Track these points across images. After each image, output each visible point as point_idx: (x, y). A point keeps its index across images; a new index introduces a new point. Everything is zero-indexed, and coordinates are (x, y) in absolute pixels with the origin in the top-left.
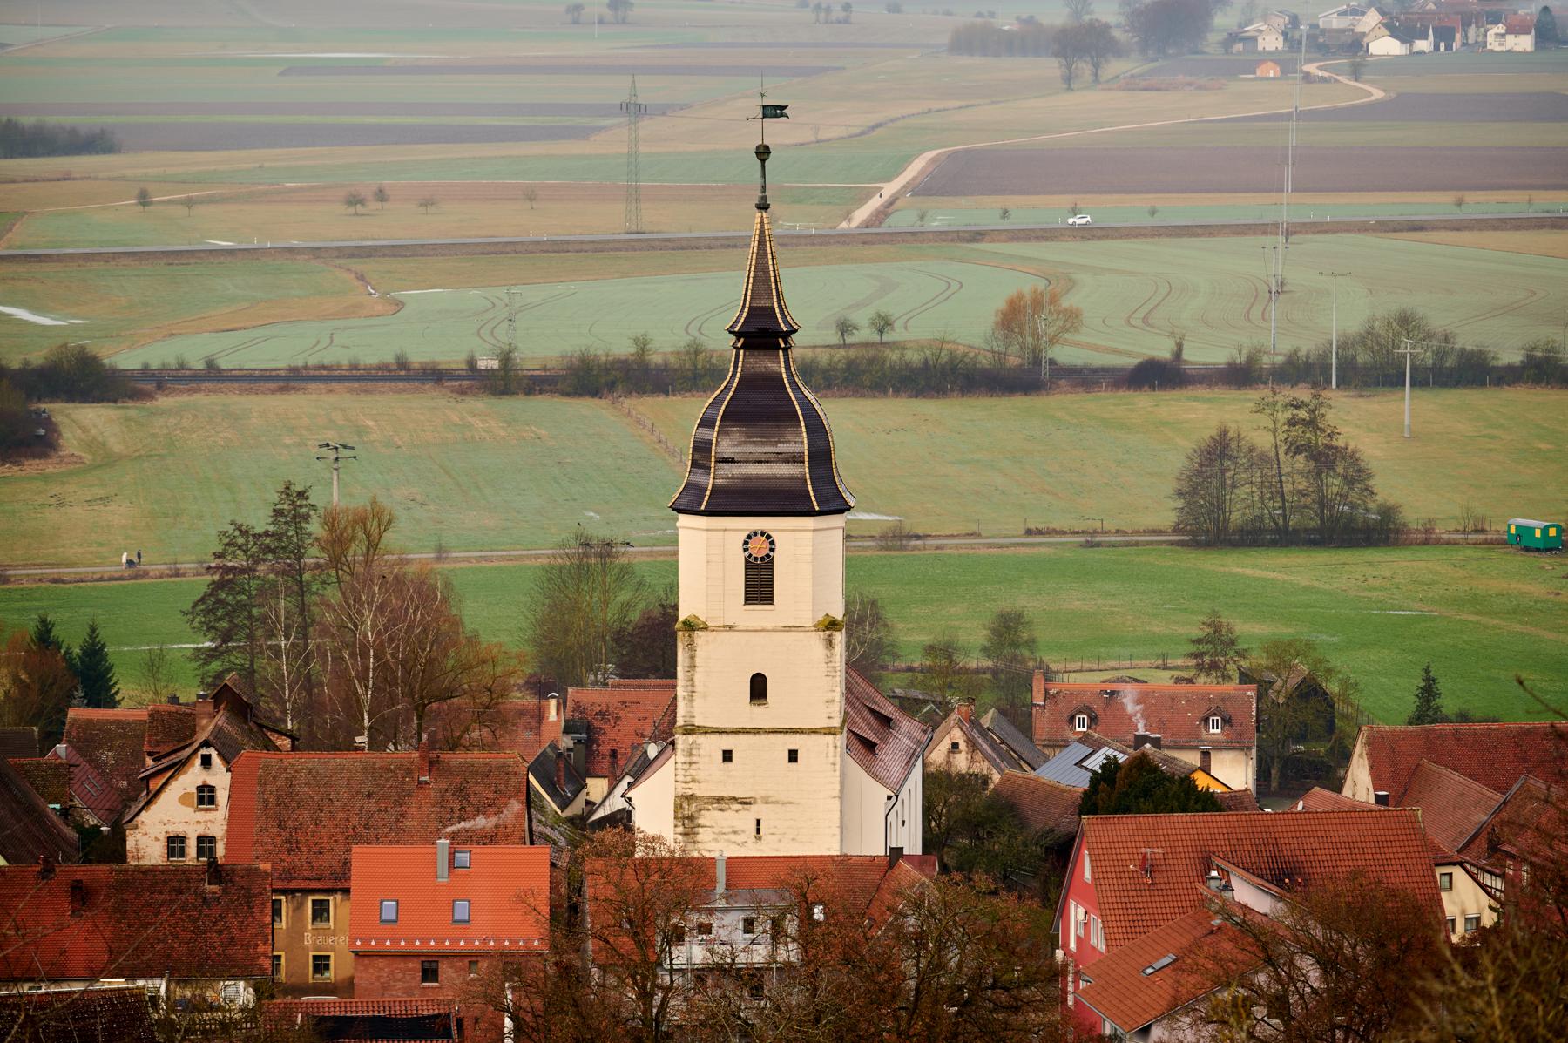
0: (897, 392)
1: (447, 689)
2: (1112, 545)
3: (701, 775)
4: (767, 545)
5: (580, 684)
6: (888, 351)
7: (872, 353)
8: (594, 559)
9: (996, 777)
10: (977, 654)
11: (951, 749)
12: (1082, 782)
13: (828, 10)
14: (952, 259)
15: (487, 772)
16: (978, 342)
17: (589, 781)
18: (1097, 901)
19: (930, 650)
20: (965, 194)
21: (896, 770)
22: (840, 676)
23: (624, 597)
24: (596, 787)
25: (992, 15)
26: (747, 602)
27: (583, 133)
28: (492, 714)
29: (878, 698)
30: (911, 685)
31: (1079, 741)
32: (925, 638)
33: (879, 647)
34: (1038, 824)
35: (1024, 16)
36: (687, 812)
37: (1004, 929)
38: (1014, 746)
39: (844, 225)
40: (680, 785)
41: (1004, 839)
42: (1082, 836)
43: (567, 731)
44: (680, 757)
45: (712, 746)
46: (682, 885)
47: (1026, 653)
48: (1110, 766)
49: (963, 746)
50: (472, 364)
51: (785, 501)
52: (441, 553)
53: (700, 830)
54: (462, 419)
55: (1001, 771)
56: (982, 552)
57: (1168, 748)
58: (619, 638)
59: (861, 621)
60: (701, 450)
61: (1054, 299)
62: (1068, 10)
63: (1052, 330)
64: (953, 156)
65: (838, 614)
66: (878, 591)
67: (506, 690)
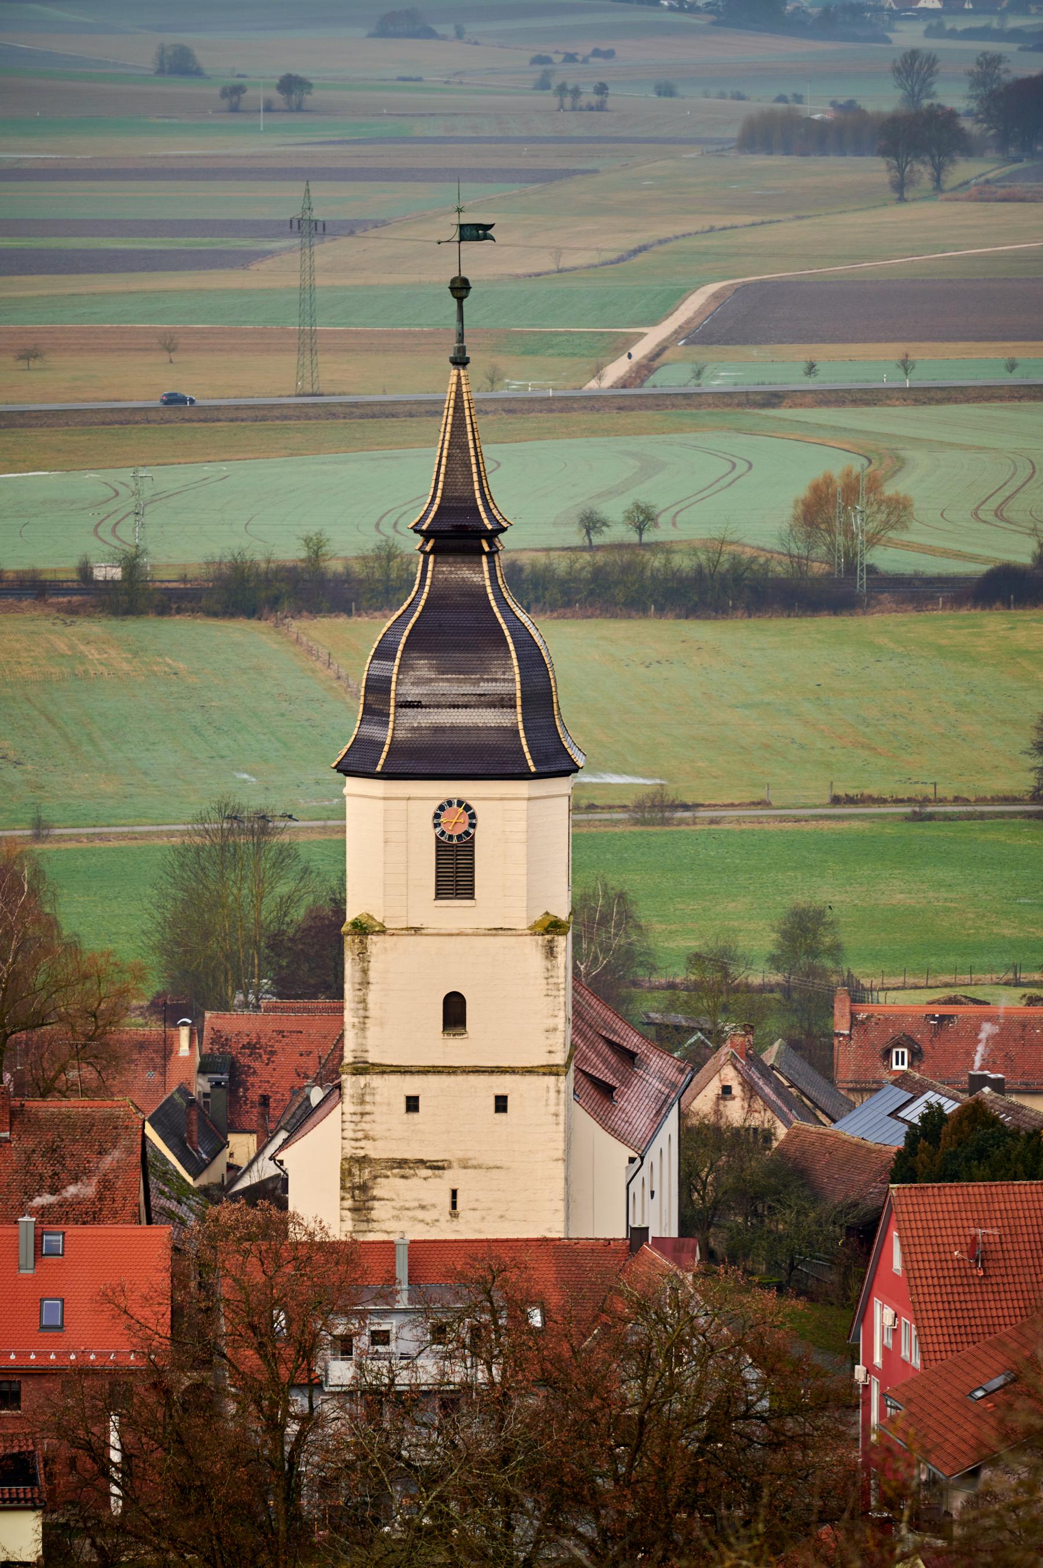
0: (661, 611)
1: (37, 1013)
2: (948, 818)
3: (376, 1130)
4: (465, 819)
5: (224, 1006)
6: (648, 555)
7: (627, 557)
8: (244, 837)
9: (781, 1131)
10: (761, 965)
11: (722, 1096)
12: (894, 1138)
13: (576, 93)
14: (739, 430)
15: (88, 1126)
16: (771, 543)
17: (232, 1138)
18: (911, 1301)
19: (696, 960)
20: (757, 343)
21: (641, 1122)
22: (564, 997)
23: (283, 888)
24: (241, 1146)
25: (798, 99)
26: (440, 894)
27: (243, 260)
28: (99, 1047)
29: (619, 1025)
30: (671, 1006)
31: (895, 1083)
32: (693, 944)
33: (628, 955)
34: (837, 1196)
35: (842, 101)
36: (358, 1181)
37: (760, 1337)
38: (808, 1089)
39: (593, 384)
40: (349, 1144)
41: (790, 1216)
42: (890, 1211)
43: (203, 1070)
44: (348, 1106)
45: (392, 1091)
46: (345, 1275)
47: (829, 964)
48: (934, 1117)
49: (737, 1090)
50: (85, 571)
51: (489, 760)
52: (40, 829)
53: (376, 1204)
54: (71, 647)
55: (787, 1123)
56: (773, 827)
57: (1018, 1092)
58: (276, 943)
59: (605, 920)
60: (377, 687)
61: (874, 485)
62: (900, 92)
63: (871, 527)
64: (742, 291)
65: (563, 913)
66: (630, 880)
67: (116, 1014)
